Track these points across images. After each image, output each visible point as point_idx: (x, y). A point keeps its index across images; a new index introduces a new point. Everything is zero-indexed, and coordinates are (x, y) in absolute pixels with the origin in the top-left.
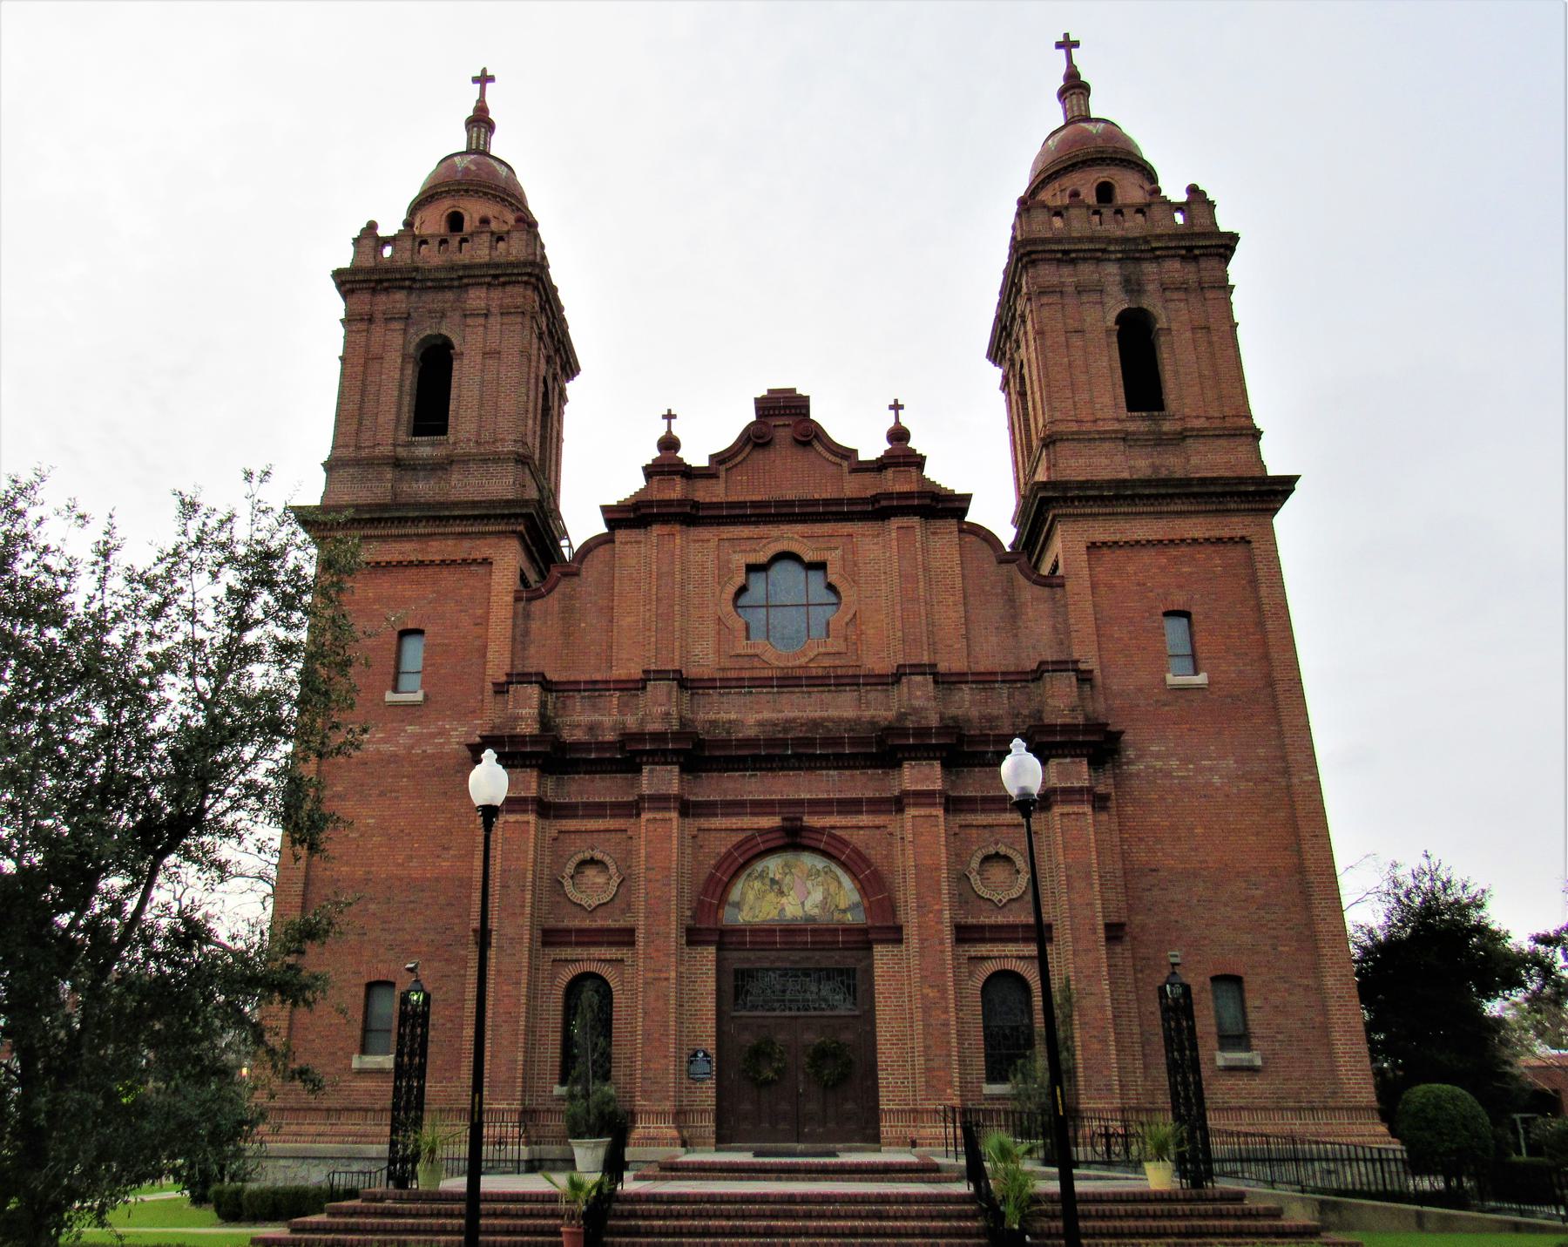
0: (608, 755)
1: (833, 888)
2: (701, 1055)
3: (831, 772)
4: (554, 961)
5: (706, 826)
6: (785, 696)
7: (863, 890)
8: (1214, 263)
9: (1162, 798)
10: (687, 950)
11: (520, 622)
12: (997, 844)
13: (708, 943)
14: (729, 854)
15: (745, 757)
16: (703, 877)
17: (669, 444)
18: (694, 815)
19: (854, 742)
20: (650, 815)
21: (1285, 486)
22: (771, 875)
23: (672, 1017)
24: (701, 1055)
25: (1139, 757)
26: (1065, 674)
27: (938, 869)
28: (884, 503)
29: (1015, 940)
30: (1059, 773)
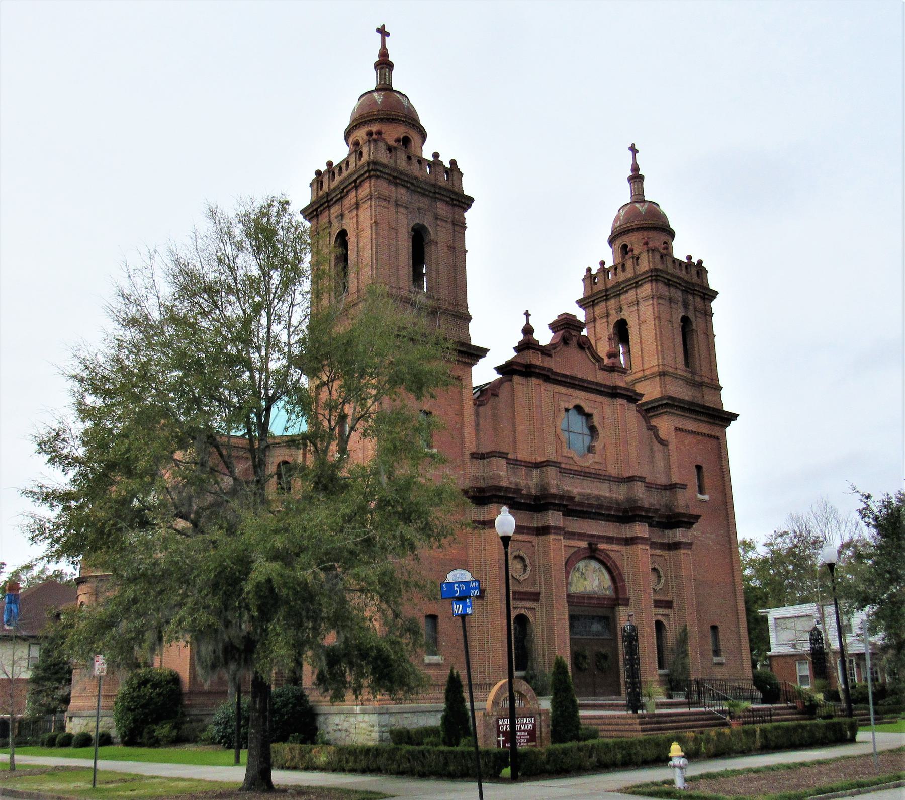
8: (461, 211)
17: (528, 331)
19: (617, 510)
21: (734, 417)
28: (619, 391)
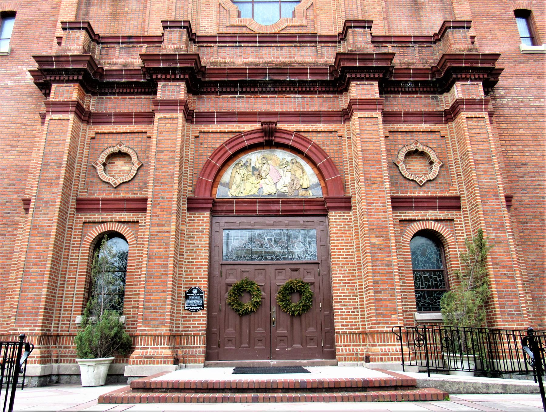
0: (134, 80)
1: (298, 173)
2: (195, 292)
3: (297, 96)
4: (85, 223)
5: (206, 130)
6: (263, 49)
7: (320, 174)
9: (524, 119)
10: (188, 214)
11: (83, 6)
12: (416, 144)
13: (204, 209)
14: (222, 148)
15: (236, 82)
16: (202, 164)
18: (197, 122)
20: (162, 115)
22: (253, 165)
23: (171, 261)
24: (195, 292)
25: (507, 94)
26: (461, 30)
27: (379, 153)
29: (433, 208)
30: (463, 91)
